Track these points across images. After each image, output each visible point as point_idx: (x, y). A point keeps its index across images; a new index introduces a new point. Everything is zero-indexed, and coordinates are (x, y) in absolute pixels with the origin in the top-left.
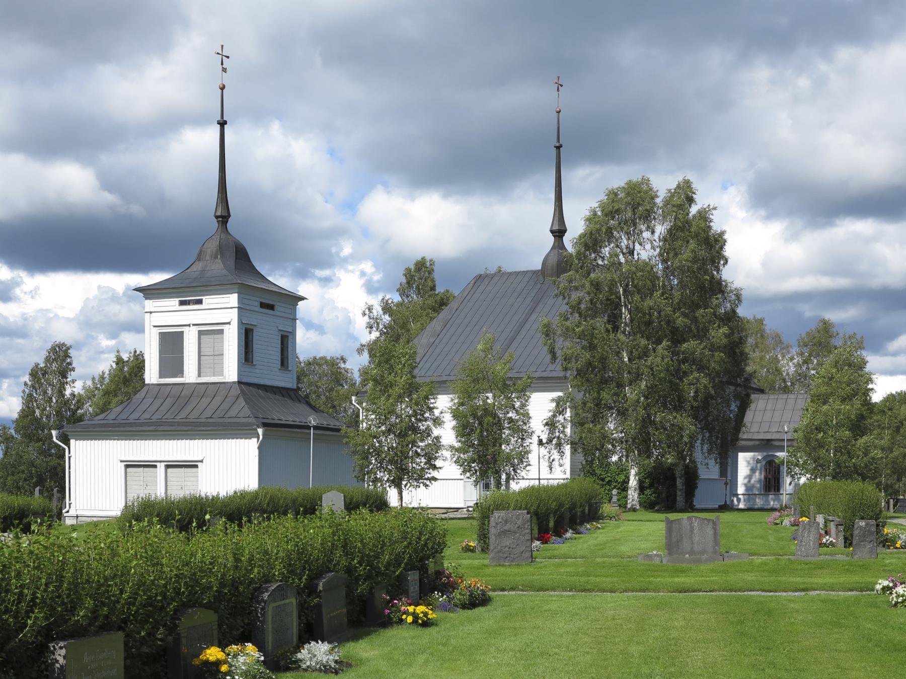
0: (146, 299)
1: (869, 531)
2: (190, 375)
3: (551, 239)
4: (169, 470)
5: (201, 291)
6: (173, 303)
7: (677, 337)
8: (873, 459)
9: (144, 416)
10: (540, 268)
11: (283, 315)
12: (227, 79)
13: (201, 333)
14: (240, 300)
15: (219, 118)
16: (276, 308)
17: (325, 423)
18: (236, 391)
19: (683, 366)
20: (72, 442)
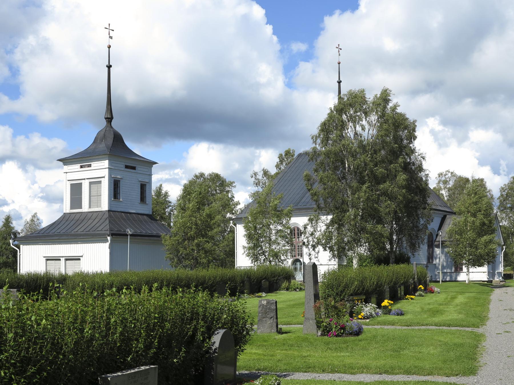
1: (269, 309)
4: (67, 262)
5: (87, 160)
6: (77, 167)
7: (377, 180)
8: (491, 249)
9: (57, 231)
11: (144, 173)
12: (112, 42)
13: (91, 183)
14: (110, 164)
16: (137, 168)
17: (138, 232)
18: (107, 215)
19: (381, 198)
20: (21, 246)
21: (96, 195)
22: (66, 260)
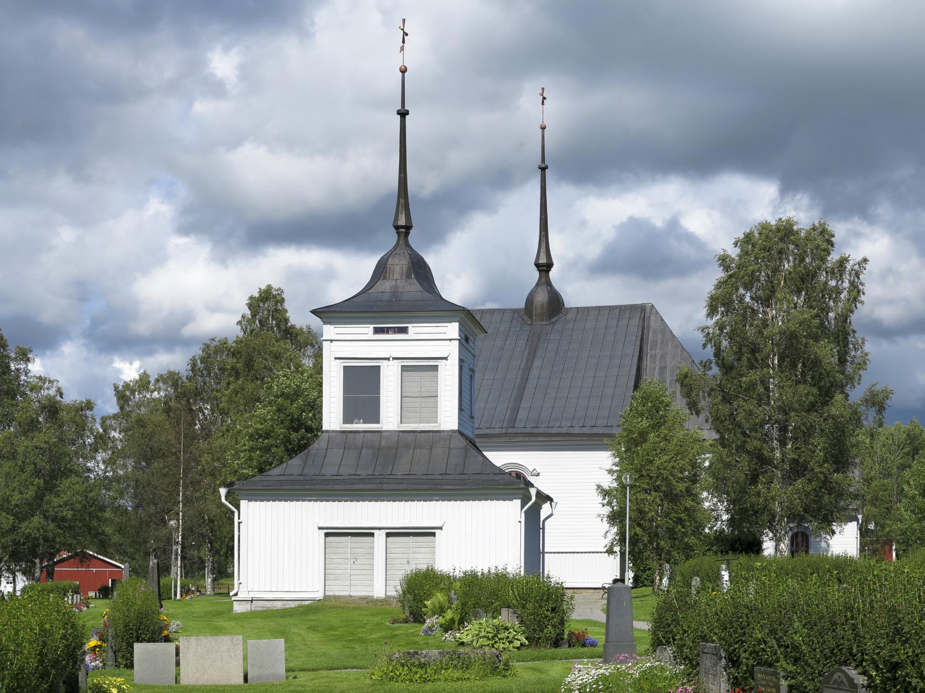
0: (325, 323)
2: (390, 418)
3: (536, 274)
5: (407, 317)
10: (522, 305)
15: (400, 108)
20: (243, 503)
21: (418, 394)
22: (388, 535)
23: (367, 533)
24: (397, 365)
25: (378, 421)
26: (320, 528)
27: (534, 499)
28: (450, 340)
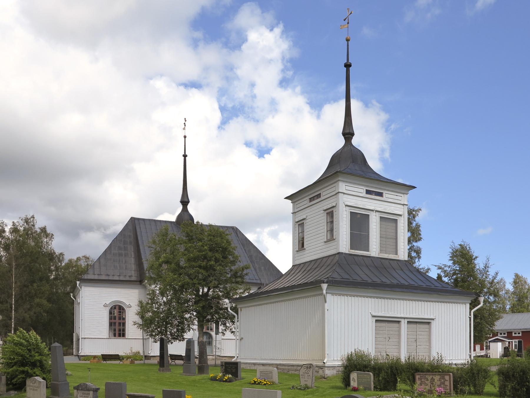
23: (396, 321)
24: (378, 215)
25: (368, 251)
26: (374, 316)
27: (482, 304)
28: (403, 205)
